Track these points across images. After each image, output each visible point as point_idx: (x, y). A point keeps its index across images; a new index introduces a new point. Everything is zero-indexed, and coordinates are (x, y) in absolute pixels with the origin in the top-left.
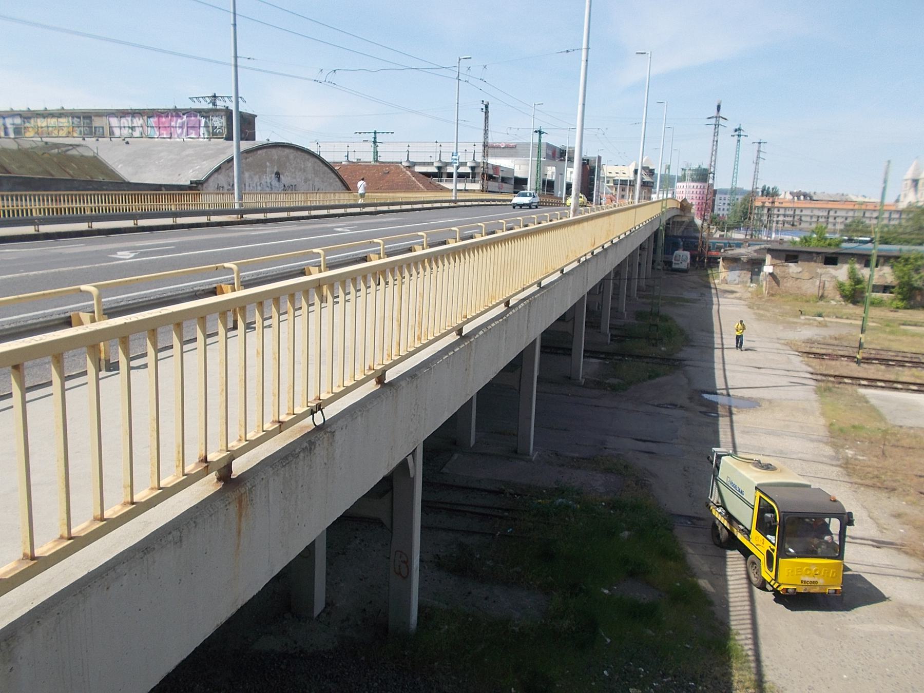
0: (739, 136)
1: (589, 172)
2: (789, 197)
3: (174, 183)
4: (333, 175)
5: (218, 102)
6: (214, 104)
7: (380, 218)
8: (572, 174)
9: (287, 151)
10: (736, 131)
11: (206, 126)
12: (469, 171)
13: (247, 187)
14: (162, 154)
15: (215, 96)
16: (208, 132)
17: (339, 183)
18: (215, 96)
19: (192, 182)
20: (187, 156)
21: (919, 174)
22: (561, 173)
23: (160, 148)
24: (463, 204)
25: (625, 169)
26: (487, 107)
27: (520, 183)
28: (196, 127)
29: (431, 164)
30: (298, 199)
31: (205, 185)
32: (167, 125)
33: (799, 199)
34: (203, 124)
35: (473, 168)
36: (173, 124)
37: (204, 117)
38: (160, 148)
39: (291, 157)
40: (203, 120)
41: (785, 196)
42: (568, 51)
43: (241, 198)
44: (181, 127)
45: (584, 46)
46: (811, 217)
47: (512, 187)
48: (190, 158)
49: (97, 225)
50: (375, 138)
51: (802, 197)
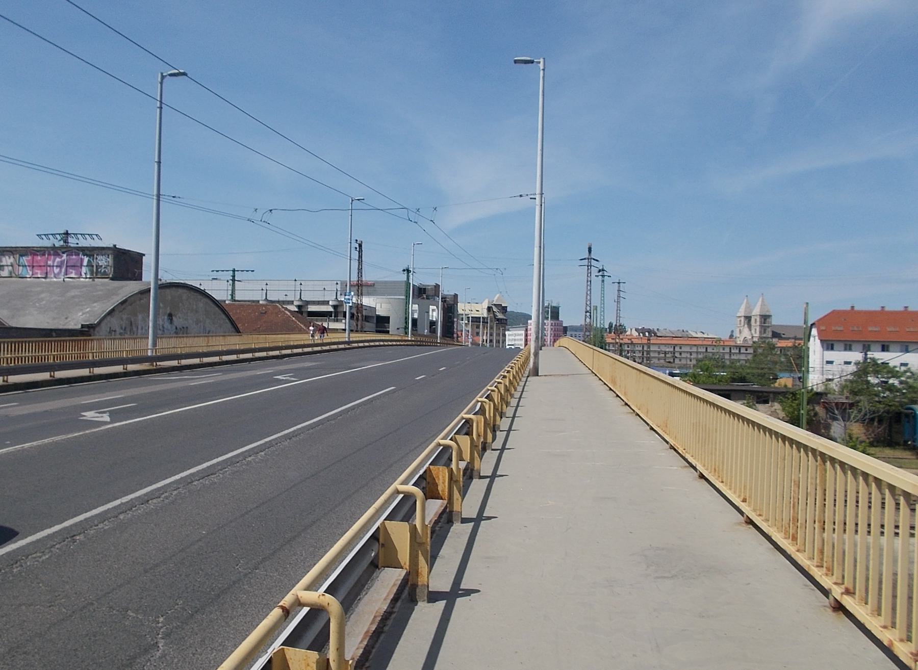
0: (603, 276)
1: (450, 309)
2: (635, 334)
3: (61, 327)
4: (224, 316)
5: (70, 240)
6: (66, 242)
7: (286, 363)
8: (435, 314)
9: (180, 291)
10: (600, 271)
11: (90, 265)
12: (331, 309)
13: (140, 331)
14: (43, 295)
15: (67, 234)
16: (92, 273)
17: (229, 325)
18: (67, 234)
19: (79, 327)
20: (73, 297)
21: (751, 311)
22: (424, 311)
23: (39, 289)
24: (356, 345)
25: (478, 307)
26: (360, 246)
27: (382, 323)
28: (77, 267)
29: (327, 303)
30: (199, 344)
31: (97, 329)
32: (42, 264)
33: (644, 335)
34: (85, 263)
35: (335, 307)
36: (50, 263)
37: (87, 256)
38: (39, 289)
39: (184, 297)
40: (86, 259)
41: (631, 332)
42: (521, 196)
43: (155, 344)
44: (59, 266)
45: (538, 191)
46: (659, 353)
47: (374, 326)
48: (77, 300)
49: (59, 374)
50: (234, 276)
51: (647, 334)
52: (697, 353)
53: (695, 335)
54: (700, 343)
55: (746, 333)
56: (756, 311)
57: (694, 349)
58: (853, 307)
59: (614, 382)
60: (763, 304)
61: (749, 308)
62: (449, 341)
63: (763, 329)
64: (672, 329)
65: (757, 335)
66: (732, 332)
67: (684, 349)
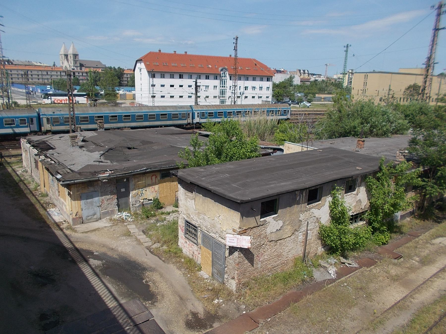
21: (68, 52)
54: (43, 69)
55: (66, 64)
56: (70, 52)
57: (40, 73)
60: (74, 48)
62: (181, 74)
63: (75, 62)
65: (72, 65)
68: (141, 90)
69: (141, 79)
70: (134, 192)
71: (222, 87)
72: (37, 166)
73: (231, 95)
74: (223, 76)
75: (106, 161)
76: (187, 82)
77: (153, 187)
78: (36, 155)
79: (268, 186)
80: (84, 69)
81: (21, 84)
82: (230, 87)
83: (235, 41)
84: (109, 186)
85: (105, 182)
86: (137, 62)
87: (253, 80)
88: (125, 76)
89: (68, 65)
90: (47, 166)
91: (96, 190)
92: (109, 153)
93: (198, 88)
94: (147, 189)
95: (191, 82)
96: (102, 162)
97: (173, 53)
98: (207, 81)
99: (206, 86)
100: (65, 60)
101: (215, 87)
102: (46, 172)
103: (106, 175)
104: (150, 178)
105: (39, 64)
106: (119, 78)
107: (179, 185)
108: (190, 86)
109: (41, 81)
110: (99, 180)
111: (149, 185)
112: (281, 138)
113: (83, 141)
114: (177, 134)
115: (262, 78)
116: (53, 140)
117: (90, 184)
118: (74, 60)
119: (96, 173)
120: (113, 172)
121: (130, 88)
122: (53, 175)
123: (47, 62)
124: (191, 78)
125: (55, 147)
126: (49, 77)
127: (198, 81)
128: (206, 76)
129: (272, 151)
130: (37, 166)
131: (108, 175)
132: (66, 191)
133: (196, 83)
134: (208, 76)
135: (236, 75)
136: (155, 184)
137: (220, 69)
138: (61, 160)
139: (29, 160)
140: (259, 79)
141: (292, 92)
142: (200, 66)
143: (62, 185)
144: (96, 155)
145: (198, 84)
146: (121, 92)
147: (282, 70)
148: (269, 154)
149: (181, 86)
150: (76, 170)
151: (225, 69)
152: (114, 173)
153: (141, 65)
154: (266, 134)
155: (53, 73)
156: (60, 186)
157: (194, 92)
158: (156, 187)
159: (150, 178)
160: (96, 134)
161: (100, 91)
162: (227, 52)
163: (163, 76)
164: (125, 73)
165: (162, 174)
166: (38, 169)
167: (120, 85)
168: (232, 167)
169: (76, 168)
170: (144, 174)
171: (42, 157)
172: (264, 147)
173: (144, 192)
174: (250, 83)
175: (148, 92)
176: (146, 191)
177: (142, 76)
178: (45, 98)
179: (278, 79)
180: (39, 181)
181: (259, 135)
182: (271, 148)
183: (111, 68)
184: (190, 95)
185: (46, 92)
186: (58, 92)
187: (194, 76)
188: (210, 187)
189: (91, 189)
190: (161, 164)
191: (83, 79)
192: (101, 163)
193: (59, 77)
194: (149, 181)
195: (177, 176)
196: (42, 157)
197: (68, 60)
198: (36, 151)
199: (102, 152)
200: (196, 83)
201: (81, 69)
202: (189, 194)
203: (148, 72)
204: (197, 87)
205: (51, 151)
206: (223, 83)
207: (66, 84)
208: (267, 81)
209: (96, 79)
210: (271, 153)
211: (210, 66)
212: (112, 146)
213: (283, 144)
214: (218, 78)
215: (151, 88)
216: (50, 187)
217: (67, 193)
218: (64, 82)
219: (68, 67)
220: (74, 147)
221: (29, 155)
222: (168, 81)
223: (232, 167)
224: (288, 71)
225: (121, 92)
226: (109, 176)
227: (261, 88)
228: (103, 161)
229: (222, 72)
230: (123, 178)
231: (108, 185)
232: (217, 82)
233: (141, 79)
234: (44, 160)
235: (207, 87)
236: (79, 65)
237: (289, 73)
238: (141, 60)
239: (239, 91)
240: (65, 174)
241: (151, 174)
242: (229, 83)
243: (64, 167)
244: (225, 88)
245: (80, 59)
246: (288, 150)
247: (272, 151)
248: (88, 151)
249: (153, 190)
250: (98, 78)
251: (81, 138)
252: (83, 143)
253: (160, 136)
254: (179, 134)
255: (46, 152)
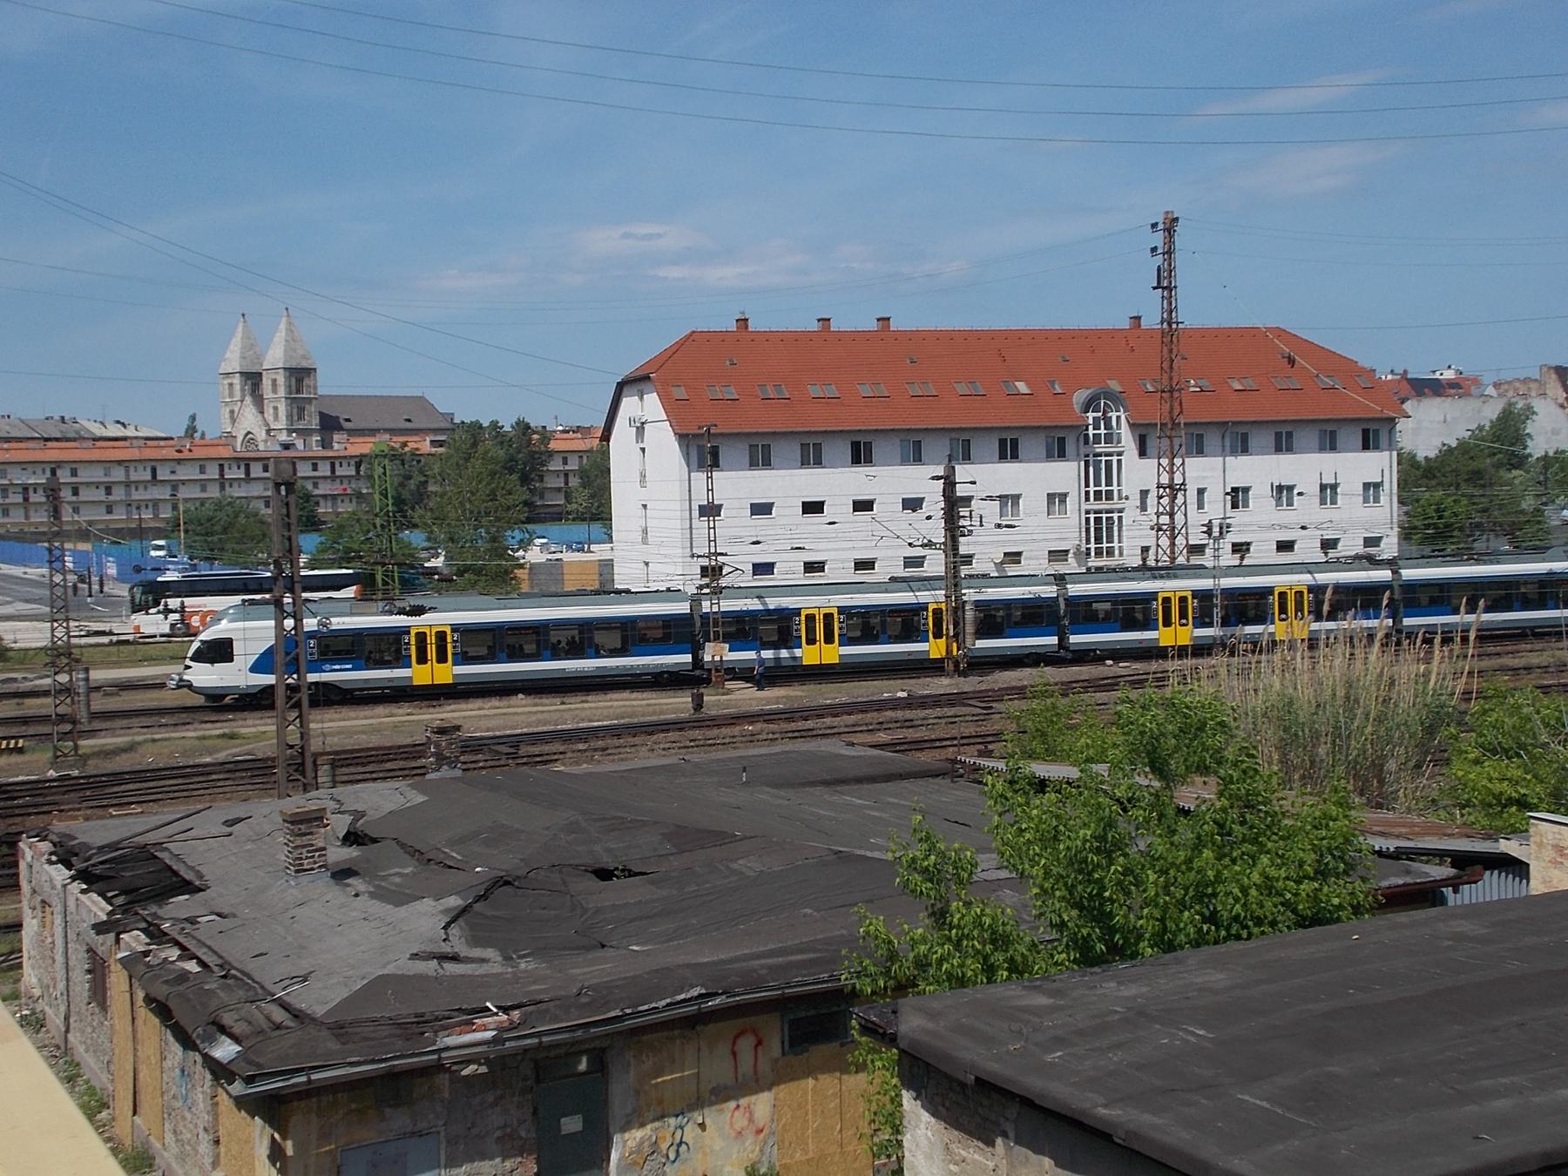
21: (259, 358)
52: (128, 484)
53: (98, 431)
54: (134, 454)
55: (249, 420)
56: (275, 357)
57: (118, 474)
58: (743, 322)
59: (259, 1066)
60: (291, 338)
61: (252, 347)
62: (862, 439)
63: (298, 406)
64: (28, 415)
65: (282, 423)
66: (193, 418)
67: (85, 475)
68: (645, 541)
69: (643, 476)
70: (636, 1135)
71: (1098, 495)
72: (99, 993)
73: (1151, 542)
74: (1097, 438)
75: (477, 953)
76: (891, 480)
77: (743, 1102)
78: (100, 928)
79: (1471, 1109)
80: (339, 444)
81: (21, 537)
82: (1144, 494)
83: (1158, 239)
84: (495, 1104)
85: (474, 1076)
86: (621, 389)
87: (1278, 450)
88: (555, 465)
89: (258, 426)
90: (161, 991)
91: (422, 1125)
92: (491, 907)
93: (964, 512)
94: (710, 1116)
95: (922, 479)
96: (455, 958)
97: (815, 326)
98: (1009, 469)
99: (1003, 498)
100: (248, 399)
101: (1056, 500)
102: (150, 1023)
103: (479, 1036)
104: (723, 1049)
105: (114, 431)
106: (525, 479)
107: (907, 1097)
108: (913, 504)
109: (119, 515)
110: (439, 1067)
111: (721, 1094)
112: (1498, 787)
113: (353, 838)
114: (859, 780)
115: (1333, 434)
116: (199, 837)
117: (392, 1089)
118: (291, 401)
119: (421, 1025)
120: (516, 1014)
121: (579, 530)
122: (187, 1042)
123: (153, 418)
124: (918, 460)
125: (201, 877)
126: (164, 493)
127: (962, 472)
128: (1002, 442)
129: (1445, 871)
130: (99, 993)
131: (489, 1034)
132: (259, 1134)
133: (949, 483)
134: (1015, 443)
135: (1175, 425)
136: (756, 1084)
137: (1079, 397)
138: (237, 950)
139: (59, 958)
140: (1315, 443)
141: (1528, 503)
142: (962, 389)
143: (240, 1102)
144: (425, 919)
145: (961, 491)
146: (535, 555)
147: (1449, 375)
148: (1427, 895)
149: (863, 506)
150: (319, 1011)
151: (1109, 395)
152: (523, 1023)
153: (647, 407)
154: (1392, 765)
155: (184, 473)
156: (225, 1101)
157: (939, 536)
158: (762, 1104)
159: (723, 1049)
160: (421, 799)
161: (424, 555)
162: (1117, 299)
163: (761, 458)
164: (551, 454)
165: (794, 1024)
166: (104, 1007)
167: (536, 515)
168: (1217, 978)
169: (319, 999)
170: (693, 1022)
171: (135, 940)
172: (1391, 845)
173: (690, 1133)
174: (1258, 470)
175: (679, 551)
176: (702, 1126)
177: (647, 467)
178: (137, 608)
179: (1429, 429)
180: (104, 1077)
181: (1353, 769)
182: (1439, 855)
183: (476, 428)
184: (919, 552)
185: (150, 576)
186: (205, 570)
187: (940, 447)
188: (1106, 1112)
189: (400, 1120)
190: (790, 965)
191: (334, 497)
192: (451, 968)
193: (213, 492)
194: (718, 1068)
195: (892, 1040)
196: (135, 940)
197: (259, 401)
198: (97, 907)
199: (454, 901)
200: (949, 483)
201: (326, 444)
202: (972, 1152)
203: (682, 438)
204: (954, 505)
205: (180, 904)
206: (1100, 472)
207: (243, 530)
208: (1366, 447)
209: (407, 493)
210: (1445, 882)
211: (1022, 387)
212: (508, 861)
213: (1518, 831)
214: (1070, 447)
215: (701, 525)
216: (167, 1112)
217: (263, 1150)
218: (242, 520)
219: (261, 435)
220: (304, 879)
221: (59, 931)
222: (787, 484)
223: (1217, 978)
224: (1488, 378)
225: (535, 555)
226: (494, 1041)
227: (1328, 492)
228: (463, 949)
229: (1091, 415)
230: (571, 1051)
231: (490, 1098)
232: (1065, 474)
233: (643, 476)
234: (146, 954)
235: (1009, 501)
236: (315, 423)
237: (1490, 391)
238: (646, 378)
239: (1197, 519)
240: (262, 1031)
241: (730, 1026)
242: (1138, 473)
243: (257, 993)
244: (1115, 504)
245: (320, 392)
246: (1555, 863)
247: (1445, 871)
248: (380, 895)
249: (741, 1121)
250: (412, 484)
251: (341, 824)
252: (353, 852)
253: (765, 795)
254: (872, 779)
255: (154, 908)
